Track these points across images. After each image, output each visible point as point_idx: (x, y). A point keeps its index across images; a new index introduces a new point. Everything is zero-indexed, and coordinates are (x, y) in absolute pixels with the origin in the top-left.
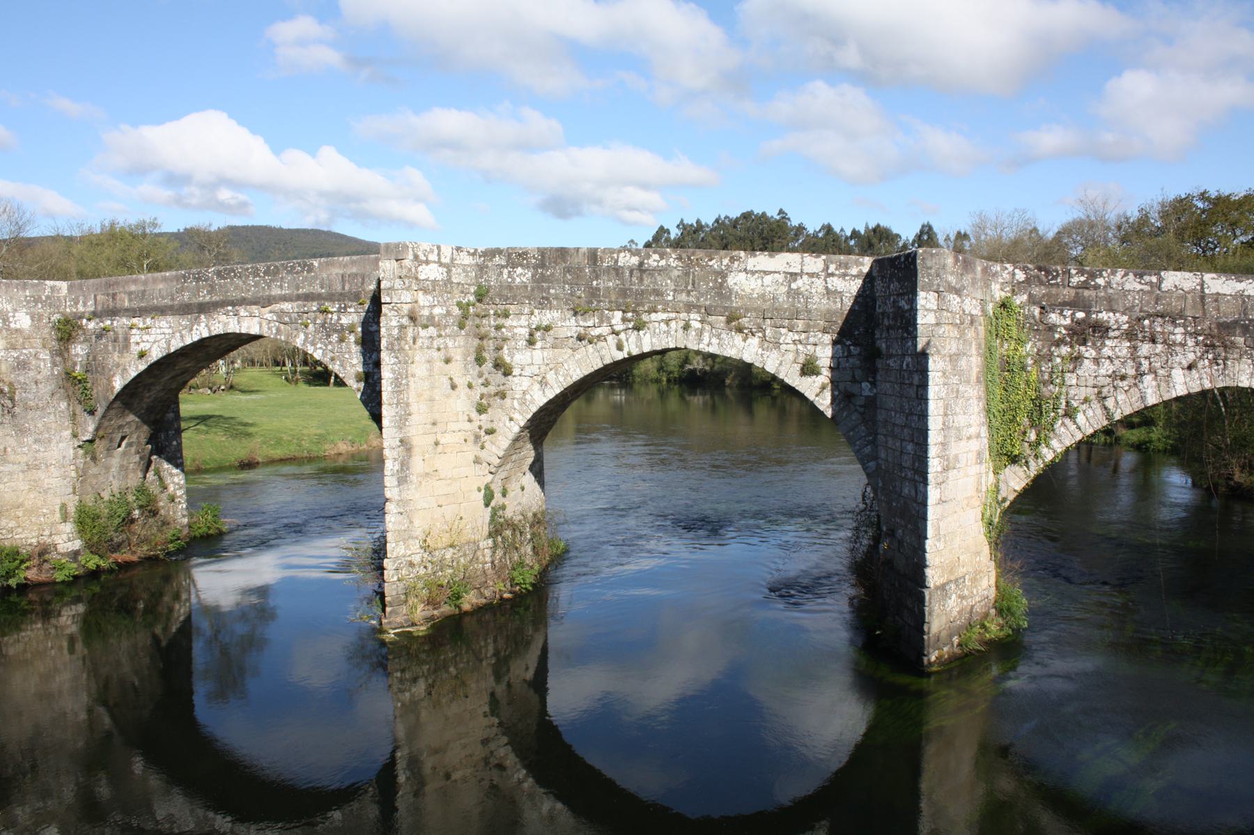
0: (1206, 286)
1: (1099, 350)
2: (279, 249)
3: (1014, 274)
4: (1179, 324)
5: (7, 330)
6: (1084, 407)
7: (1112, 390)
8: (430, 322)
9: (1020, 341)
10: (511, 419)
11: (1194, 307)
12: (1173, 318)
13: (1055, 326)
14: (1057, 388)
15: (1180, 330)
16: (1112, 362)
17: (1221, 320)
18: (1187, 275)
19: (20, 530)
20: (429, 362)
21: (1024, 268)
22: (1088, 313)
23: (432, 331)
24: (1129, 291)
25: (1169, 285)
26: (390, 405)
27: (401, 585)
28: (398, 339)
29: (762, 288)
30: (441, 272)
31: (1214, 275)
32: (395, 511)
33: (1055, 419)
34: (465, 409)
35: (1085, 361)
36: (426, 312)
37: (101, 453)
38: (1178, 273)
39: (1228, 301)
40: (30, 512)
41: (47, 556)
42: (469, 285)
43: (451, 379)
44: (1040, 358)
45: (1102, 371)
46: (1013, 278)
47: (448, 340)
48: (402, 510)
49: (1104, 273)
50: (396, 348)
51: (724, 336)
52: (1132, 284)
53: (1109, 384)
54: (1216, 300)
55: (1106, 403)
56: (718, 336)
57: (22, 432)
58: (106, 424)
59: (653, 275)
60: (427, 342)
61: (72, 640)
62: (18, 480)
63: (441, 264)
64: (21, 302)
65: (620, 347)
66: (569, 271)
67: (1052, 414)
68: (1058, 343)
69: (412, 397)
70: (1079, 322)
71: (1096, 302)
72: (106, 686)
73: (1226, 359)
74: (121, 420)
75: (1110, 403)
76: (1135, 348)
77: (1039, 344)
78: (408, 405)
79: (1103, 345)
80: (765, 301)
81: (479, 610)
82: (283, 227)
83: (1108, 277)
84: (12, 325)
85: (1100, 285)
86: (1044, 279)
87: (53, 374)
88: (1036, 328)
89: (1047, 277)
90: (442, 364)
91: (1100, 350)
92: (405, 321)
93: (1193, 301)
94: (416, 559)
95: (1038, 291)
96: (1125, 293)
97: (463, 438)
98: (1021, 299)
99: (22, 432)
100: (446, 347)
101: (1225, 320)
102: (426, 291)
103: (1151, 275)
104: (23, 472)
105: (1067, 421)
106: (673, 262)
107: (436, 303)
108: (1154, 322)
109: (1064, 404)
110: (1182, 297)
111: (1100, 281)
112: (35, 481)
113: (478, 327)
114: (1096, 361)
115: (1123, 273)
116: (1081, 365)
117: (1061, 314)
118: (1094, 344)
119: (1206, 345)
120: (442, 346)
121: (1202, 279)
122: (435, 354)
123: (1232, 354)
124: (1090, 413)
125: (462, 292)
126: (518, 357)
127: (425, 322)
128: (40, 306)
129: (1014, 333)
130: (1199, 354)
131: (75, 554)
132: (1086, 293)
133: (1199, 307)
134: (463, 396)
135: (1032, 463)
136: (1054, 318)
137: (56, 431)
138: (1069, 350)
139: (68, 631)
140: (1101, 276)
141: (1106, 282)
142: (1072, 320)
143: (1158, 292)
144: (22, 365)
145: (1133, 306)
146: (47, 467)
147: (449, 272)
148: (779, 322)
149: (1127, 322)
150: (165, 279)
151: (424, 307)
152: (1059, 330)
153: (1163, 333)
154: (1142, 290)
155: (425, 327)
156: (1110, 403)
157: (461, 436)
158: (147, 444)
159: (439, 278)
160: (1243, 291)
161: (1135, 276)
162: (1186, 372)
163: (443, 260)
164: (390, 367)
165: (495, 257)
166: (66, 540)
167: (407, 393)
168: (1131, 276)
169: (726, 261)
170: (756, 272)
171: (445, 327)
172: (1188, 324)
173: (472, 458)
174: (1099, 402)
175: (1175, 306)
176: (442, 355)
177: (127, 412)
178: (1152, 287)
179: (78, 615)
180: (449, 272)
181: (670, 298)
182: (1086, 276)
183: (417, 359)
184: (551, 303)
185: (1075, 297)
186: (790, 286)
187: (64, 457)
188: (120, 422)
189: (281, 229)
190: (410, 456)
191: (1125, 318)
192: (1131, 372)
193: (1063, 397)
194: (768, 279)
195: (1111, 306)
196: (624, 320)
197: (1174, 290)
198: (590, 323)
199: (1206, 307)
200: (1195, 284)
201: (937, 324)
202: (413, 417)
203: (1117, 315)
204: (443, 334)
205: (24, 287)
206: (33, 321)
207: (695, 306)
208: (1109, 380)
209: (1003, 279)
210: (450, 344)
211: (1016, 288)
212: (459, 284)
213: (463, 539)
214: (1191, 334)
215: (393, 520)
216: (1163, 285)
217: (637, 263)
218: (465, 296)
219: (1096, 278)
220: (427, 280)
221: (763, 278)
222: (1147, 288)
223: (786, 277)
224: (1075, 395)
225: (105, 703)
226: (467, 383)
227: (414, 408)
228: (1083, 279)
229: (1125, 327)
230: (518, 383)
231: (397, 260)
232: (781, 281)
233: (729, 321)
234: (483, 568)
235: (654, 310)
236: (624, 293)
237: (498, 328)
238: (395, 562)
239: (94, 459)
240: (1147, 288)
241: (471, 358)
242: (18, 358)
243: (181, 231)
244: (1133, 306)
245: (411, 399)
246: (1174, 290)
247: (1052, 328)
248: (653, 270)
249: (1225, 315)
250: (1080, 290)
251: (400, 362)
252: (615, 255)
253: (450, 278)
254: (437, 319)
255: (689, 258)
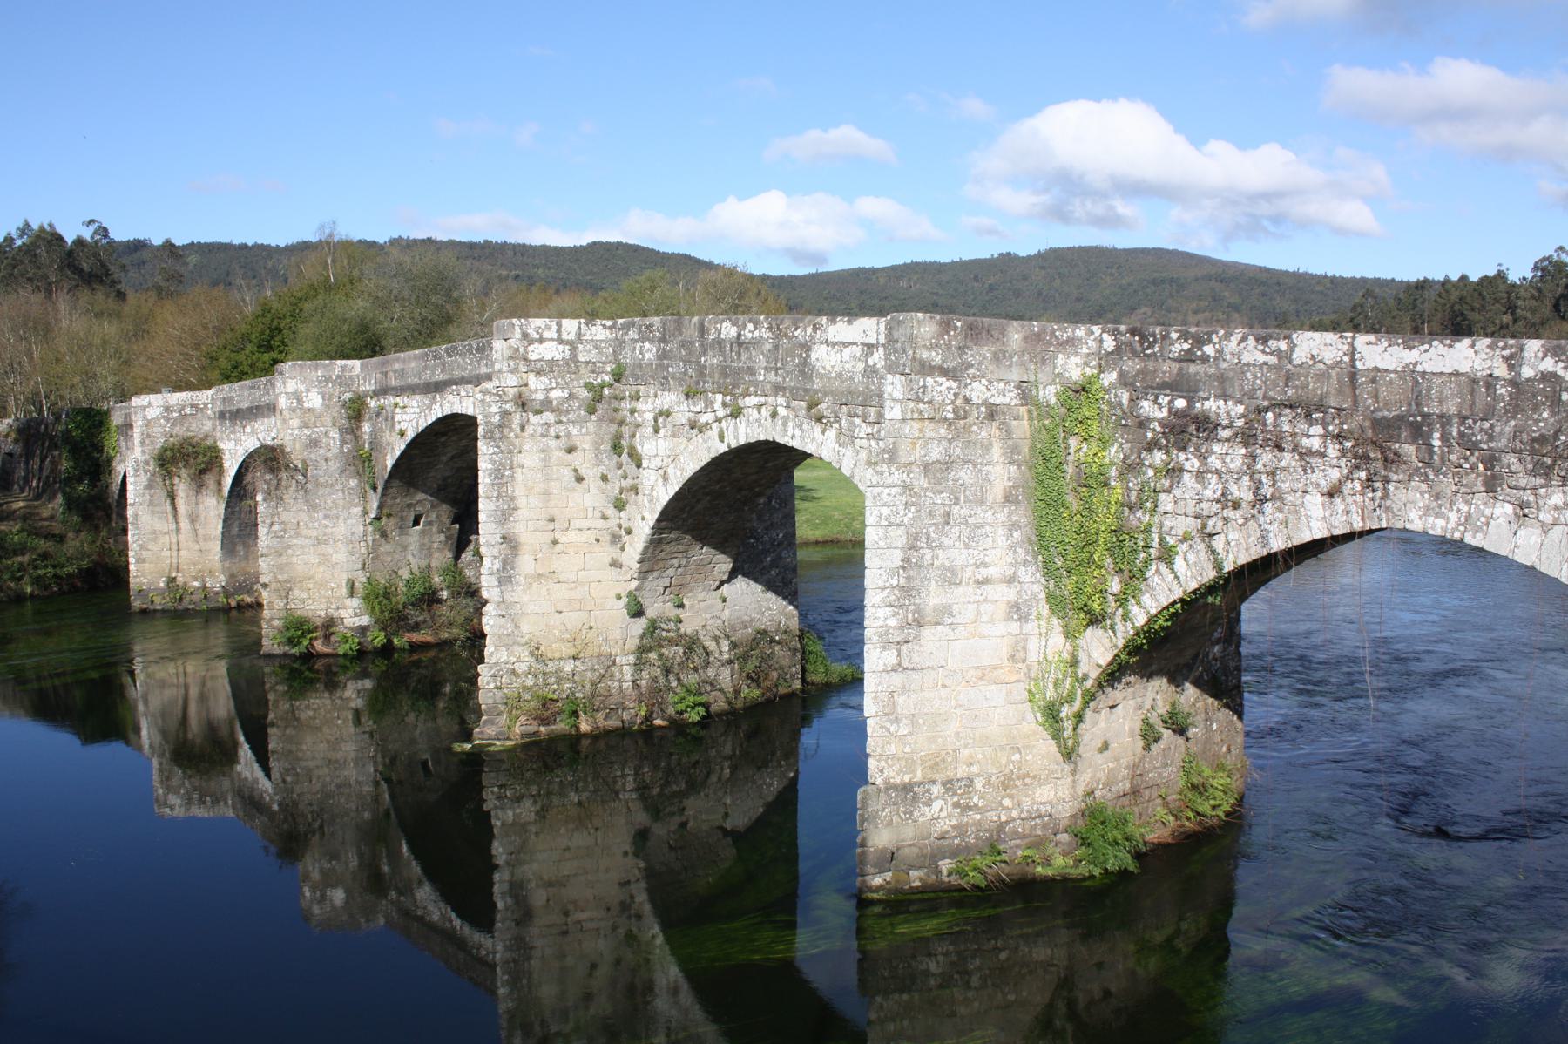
0: (1358, 356)
1: (1203, 458)
2: (1112, 275)
3: (1101, 341)
4: (1316, 420)
5: (301, 409)
6: (1184, 547)
7: (1220, 523)
8: (546, 405)
9: (1104, 443)
10: (643, 519)
11: (1340, 392)
12: (1308, 409)
13: (1149, 420)
14: (1148, 516)
15: (1317, 430)
16: (1220, 478)
17: (1379, 415)
18: (1330, 337)
19: (311, 602)
20: (543, 451)
21: (1113, 331)
22: (1191, 401)
23: (548, 416)
24: (1248, 365)
25: (1303, 355)
26: (488, 498)
27: (499, 694)
28: (500, 426)
29: (841, 365)
30: (561, 351)
31: (1371, 338)
32: (494, 613)
33: (1147, 564)
34: (596, 505)
35: (1186, 476)
36: (540, 396)
37: (393, 531)
38: (1317, 335)
39: (1391, 382)
40: (322, 585)
41: (334, 629)
42: (604, 363)
43: (576, 470)
44: (1130, 468)
45: (1208, 493)
46: (1100, 347)
47: (571, 427)
48: (504, 613)
49: (1214, 336)
50: (498, 435)
51: (805, 426)
52: (1253, 354)
53: (1216, 514)
54: (1373, 381)
55: (1214, 543)
56: (800, 426)
57: (313, 507)
58: (389, 502)
59: (748, 349)
60: (539, 430)
61: (357, 713)
62: (309, 553)
63: (561, 342)
64: (313, 381)
65: (722, 438)
66: (683, 346)
67: (1143, 555)
68: (1151, 446)
69: (519, 491)
70: (1180, 414)
71: (1205, 382)
72: (393, 760)
73: (1386, 481)
74: (408, 498)
75: (1218, 543)
76: (1253, 457)
77: (1127, 446)
78: (512, 499)
79: (1210, 452)
80: (842, 382)
81: (598, 736)
82: (1116, 246)
83: (1220, 343)
84: (306, 405)
85: (1209, 356)
86: (1138, 347)
87: (342, 452)
88: (1123, 422)
89: (1142, 344)
90: (562, 454)
91: (1205, 458)
92: (509, 407)
93: (1339, 382)
94: (522, 667)
95: (1131, 366)
96: (1242, 368)
97: (593, 537)
98: (1110, 378)
99: (313, 507)
100: (569, 435)
101: (1386, 413)
102: (539, 373)
103: (1278, 340)
104: (314, 546)
105: (1163, 567)
106: (766, 334)
107: (554, 385)
108: (1280, 415)
109: (1157, 540)
110: (1323, 375)
111: (1209, 350)
112: (324, 555)
113: (616, 410)
114: (1200, 476)
115: (1240, 336)
116: (1178, 483)
117: (1155, 402)
118: (1197, 449)
119: (1356, 456)
120: (562, 434)
121: (1352, 344)
122: (553, 443)
123: (1396, 473)
124: (1191, 557)
125: (593, 372)
126: (649, 447)
127: (538, 407)
128: (330, 385)
129: (1095, 428)
130: (1346, 471)
131: (363, 630)
132: (1193, 368)
133: (1348, 390)
134: (594, 490)
135: (1119, 626)
136: (1146, 407)
137: (344, 508)
138: (1164, 457)
139: (353, 705)
140: (1210, 341)
141: (1217, 351)
142: (1170, 411)
143: (1289, 366)
144: (314, 443)
145: (1254, 390)
146: (335, 542)
147: (574, 350)
148: (853, 409)
149: (1243, 416)
150: (416, 357)
151: (536, 390)
152: (1152, 426)
153: (1294, 435)
154: (1265, 363)
155: (538, 412)
156: (1218, 543)
157: (591, 535)
158: (453, 523)
159: (559, 356)
160: (1415, 365)
161: (1257, 340)
162: (1326, 499)
163: (565, 336)
164: (487, 457)
165: (629, 330)
166: (353, 615)
167: (512, 486)
168: (1251, 340)
169: (809, 330)
170: (836, 343)
171: (568, 412)
172: (1329, 420)
173: (608, 560)
174: (1204, 541)
175: (1313, 390)
176: (562, 442)
177: (412, 490)
178: (1279, 359)
179: (365, 690)
180: (574, 350)
181: (761, 378)
182: (1190, 341)
183: (526, 447)
184: (668, 383)
185: (1178, 374)
186: (867, 361)
187: (353, 534)
188: (408, 501)
189: (1115, 249)
190: (516, 555)
191: (1241, 409)
192: (1248, 496)
193: (1154, 530)
194: (847, 351)
195: (1224, 389)
196: (724, 405)
197: (1311, 363)
198: (698, 409)
199: (1358, 392)
200: (1341, 353)
201: (904, 420)
202: (519, 512)
203: (1230, 403)
204: (565, 419)
205: (316, 369)
206: (324, 399)
207: (784, 389)
208: (1216, 507)
209: (1088, 348)
210: (574, 431)
211: (1106, 360)
212: (588, 363)
213: (590, 651)
214: (1333, 437)
215: (491, 622)
216: (1295, 356)
217: (735, 334)
218: (597, 377)
219: (1204, 344)
220: (540, 360)
221: (842, 351)
222: (1272, 360)
223: (863, 350)
224: (1172, 528)
225: (388, 781)
226: (600, 475)
227: (521, 502)
228: (1186, 346)
229: (1240, 423)
230: (648, 477)
231: (506, 340)
232: (858, 355)
233: (810, 407)
234: (621, 687)
235: (746, 394)
236: (724, 372)
237: (633, 411)
238: (491, 668)
239: (384, 535)
240: (1272, 360)
241: (607, 446)
242: (310, 436)
243: (996, 256)
244: (1254, 390)
245: (517, 492)
246: (1311, 363)
247: (1143, 423)
248: (749, 343)
249: (1387, 407)
250: (1185, 364)
251: (502, 452)
252: (718, 326)
253: (575, 356)
254: (555, 403)
255: (778, 328)
